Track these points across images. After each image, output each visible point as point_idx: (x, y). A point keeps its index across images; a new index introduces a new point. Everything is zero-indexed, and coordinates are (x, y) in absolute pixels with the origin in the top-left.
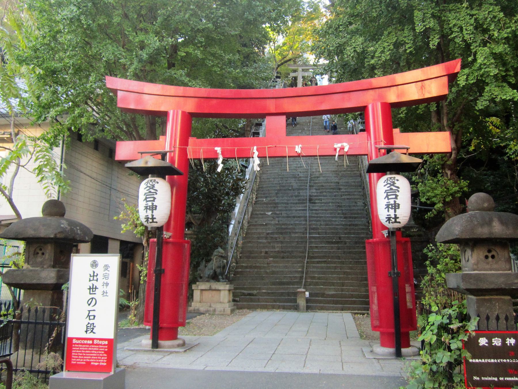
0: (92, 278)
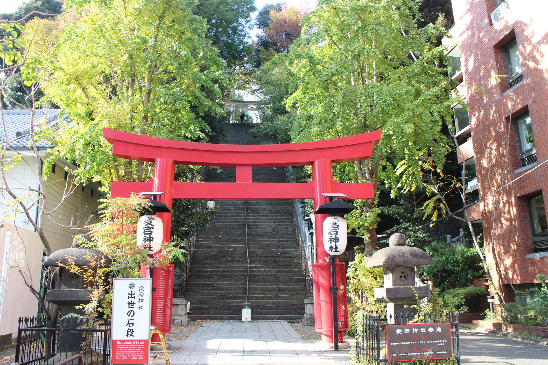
0: (130, 296)
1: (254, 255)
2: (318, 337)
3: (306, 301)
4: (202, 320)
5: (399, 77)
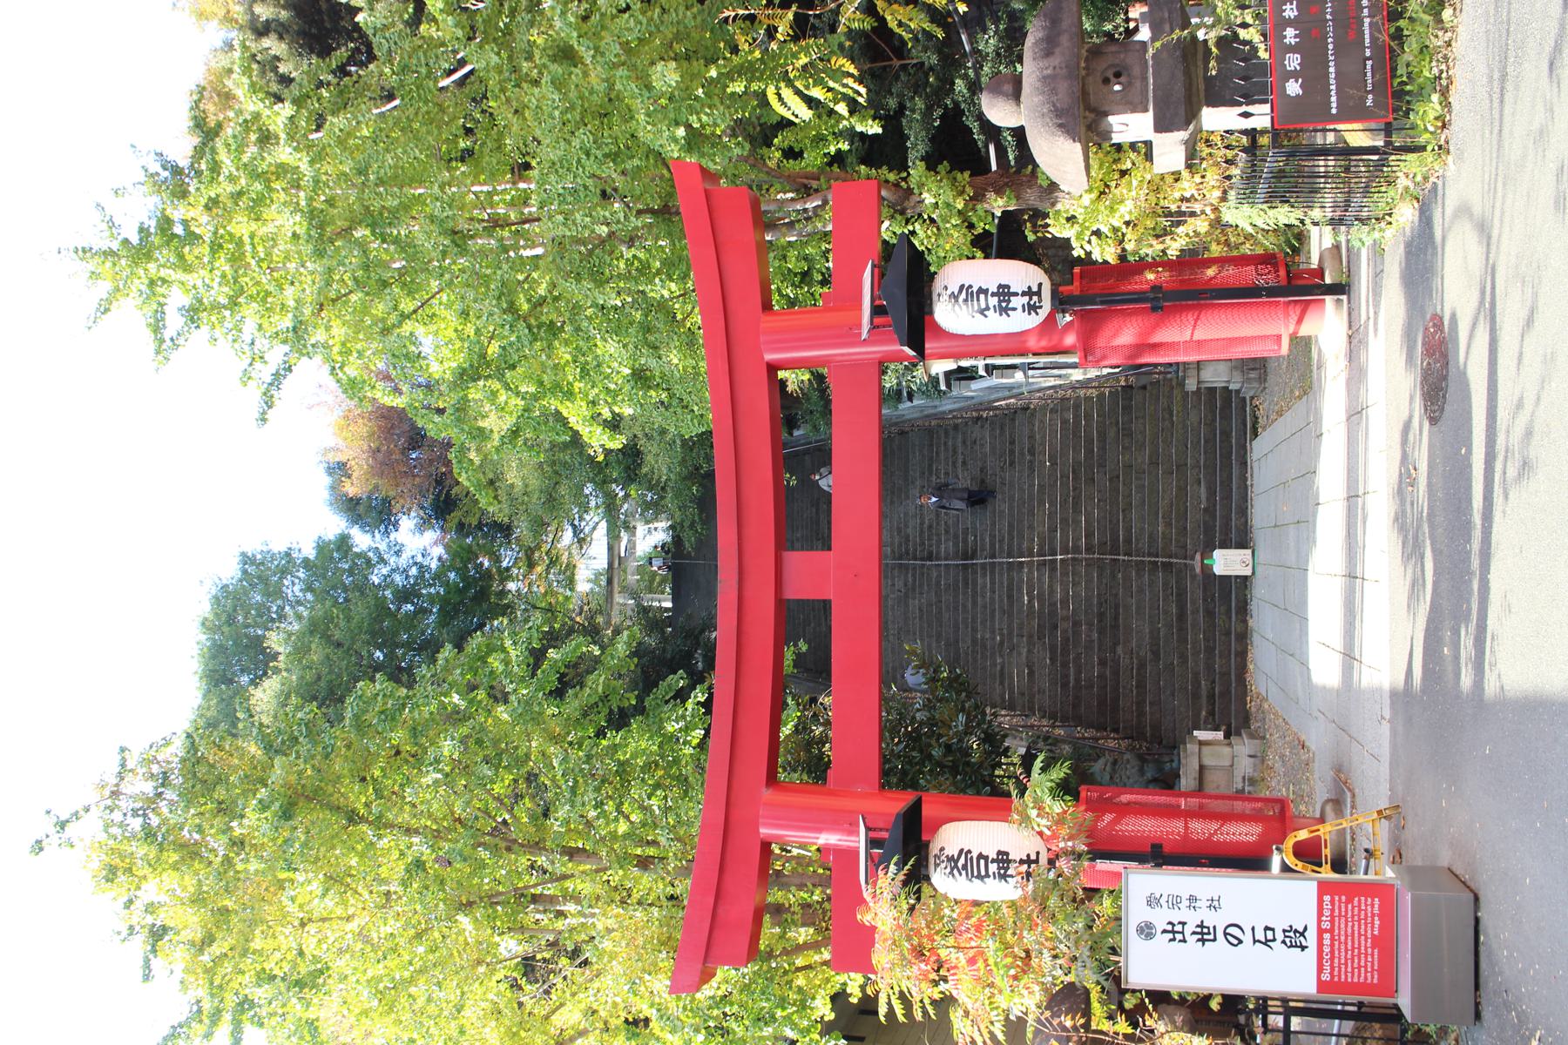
0: (1179, 937)
1: (1052, 540)
2: (1303, 345)
3: (1191, 385)
4: (1245, 694)
5: (516, 112)
